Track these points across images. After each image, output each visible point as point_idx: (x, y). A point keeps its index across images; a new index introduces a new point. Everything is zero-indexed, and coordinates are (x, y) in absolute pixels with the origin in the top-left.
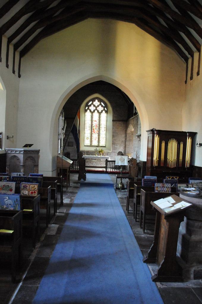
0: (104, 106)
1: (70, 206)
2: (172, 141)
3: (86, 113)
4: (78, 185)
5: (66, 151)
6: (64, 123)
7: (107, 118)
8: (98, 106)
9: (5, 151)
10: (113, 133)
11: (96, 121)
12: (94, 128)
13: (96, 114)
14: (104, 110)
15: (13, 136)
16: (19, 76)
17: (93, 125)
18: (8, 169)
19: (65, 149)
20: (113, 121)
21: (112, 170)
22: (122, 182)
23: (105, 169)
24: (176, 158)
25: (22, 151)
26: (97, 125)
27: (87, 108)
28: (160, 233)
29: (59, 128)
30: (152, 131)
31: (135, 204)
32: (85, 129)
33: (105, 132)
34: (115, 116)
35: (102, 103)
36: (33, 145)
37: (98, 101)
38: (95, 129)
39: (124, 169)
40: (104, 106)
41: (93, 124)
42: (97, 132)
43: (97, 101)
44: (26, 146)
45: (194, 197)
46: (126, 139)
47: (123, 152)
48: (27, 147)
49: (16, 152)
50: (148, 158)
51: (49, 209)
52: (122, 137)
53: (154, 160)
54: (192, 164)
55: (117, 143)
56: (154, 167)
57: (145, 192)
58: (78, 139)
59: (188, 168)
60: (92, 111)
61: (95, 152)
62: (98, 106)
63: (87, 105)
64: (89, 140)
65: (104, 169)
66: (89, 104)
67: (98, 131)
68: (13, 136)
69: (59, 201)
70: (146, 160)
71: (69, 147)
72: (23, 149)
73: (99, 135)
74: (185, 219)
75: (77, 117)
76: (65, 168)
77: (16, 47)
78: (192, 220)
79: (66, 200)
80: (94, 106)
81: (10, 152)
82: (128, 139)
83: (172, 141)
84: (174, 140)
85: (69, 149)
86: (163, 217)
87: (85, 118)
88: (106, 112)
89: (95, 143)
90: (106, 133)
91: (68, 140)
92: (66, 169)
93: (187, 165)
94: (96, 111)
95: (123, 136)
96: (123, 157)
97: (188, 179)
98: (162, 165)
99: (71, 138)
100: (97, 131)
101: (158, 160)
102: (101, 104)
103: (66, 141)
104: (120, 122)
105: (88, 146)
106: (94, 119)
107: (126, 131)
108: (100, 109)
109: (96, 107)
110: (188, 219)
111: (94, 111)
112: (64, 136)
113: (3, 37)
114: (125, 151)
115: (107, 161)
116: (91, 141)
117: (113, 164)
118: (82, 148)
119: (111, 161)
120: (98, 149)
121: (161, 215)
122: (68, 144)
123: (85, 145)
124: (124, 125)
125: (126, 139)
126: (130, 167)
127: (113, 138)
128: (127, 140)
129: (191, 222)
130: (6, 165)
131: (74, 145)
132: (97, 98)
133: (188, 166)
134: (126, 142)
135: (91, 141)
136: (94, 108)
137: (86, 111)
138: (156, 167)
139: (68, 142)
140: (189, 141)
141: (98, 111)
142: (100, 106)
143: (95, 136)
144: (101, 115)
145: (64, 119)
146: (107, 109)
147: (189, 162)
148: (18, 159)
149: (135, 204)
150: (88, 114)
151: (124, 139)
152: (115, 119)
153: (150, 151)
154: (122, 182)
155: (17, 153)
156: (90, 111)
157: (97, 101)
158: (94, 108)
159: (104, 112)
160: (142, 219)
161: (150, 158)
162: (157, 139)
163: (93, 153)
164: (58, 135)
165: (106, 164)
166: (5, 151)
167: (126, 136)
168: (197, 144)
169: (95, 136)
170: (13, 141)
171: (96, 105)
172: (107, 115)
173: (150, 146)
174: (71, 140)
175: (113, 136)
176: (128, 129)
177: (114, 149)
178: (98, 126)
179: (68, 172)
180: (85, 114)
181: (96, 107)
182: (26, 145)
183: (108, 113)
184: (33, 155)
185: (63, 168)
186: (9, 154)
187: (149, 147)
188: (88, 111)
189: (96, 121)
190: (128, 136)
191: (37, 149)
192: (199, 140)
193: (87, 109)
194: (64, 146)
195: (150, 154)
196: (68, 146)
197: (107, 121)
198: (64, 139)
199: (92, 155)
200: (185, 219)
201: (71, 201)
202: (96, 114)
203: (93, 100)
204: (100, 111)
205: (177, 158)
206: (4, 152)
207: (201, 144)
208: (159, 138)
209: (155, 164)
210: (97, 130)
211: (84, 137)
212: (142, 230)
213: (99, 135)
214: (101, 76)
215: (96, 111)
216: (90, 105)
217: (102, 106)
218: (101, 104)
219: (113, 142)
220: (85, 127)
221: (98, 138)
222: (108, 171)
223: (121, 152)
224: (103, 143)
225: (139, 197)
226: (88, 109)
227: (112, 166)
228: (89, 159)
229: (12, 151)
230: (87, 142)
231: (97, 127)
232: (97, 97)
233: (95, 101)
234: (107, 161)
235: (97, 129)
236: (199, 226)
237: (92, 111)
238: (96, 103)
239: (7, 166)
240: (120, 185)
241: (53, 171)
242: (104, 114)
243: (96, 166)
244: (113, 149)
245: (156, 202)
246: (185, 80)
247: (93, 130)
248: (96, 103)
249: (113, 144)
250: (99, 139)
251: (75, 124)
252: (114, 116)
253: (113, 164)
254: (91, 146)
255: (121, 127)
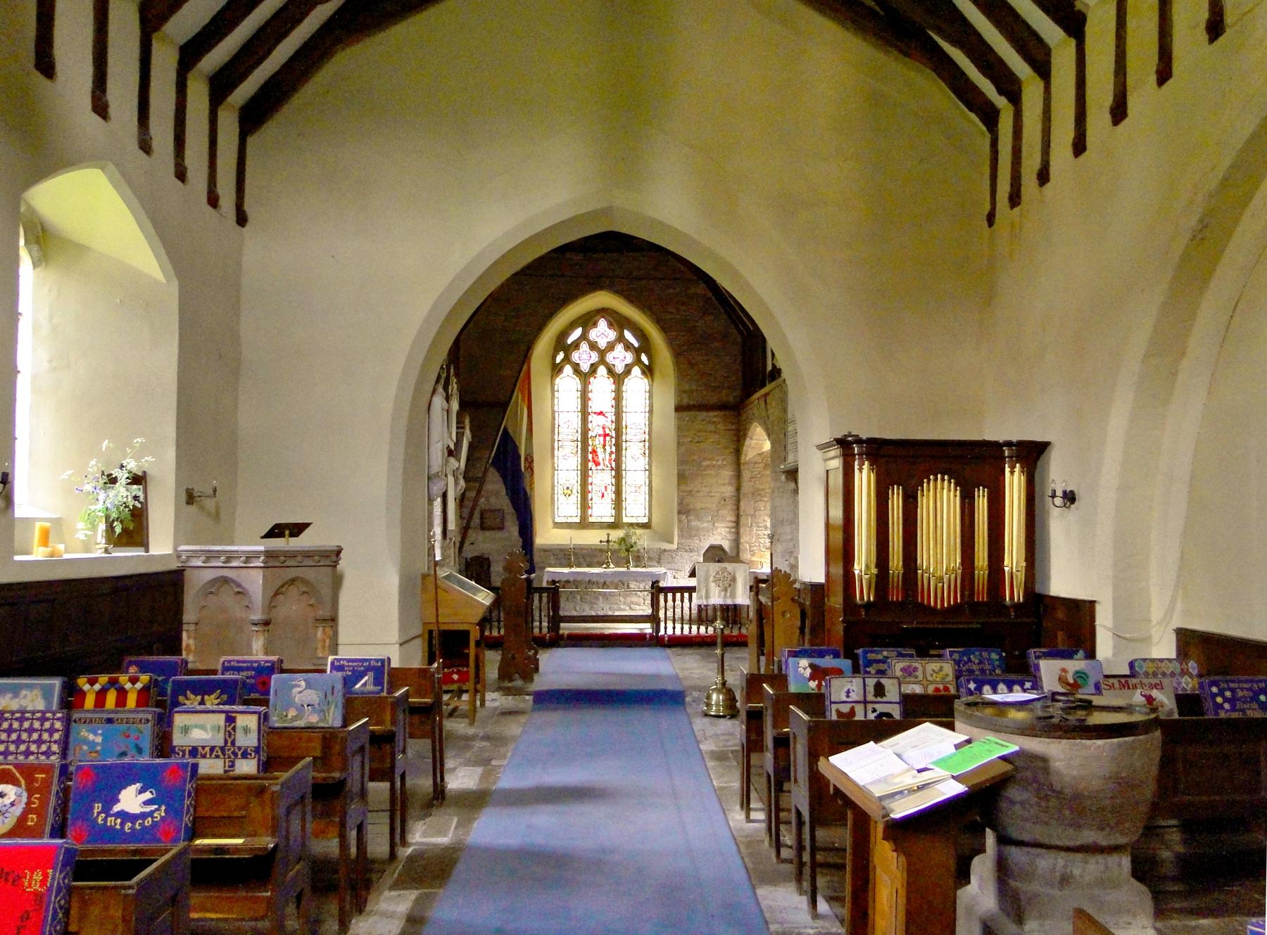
0: (636, 345)
1: (474, 801)
2: (936, 489)
3: (558, 380)
4: (525, 701)
5: (470, 552)
6: (460, 426)
7: (651, 397)
8: (611, 347)
9: (179, 557)
10: (682, 462)
11: (601, 413)
12: (597, 442)
13: (602, 386)
14: (638, 361)
15: (215, 491)
16: (242, 219)
17: (590, 434)
18: (191, 642)
19: (467, 543)
20: (679, 409)
21: (686, 627)
22: (724, 684)
23: (648, 625)
24: (959, 561)
25: (256, 555)
26: (607, 431)
27: (560, 357)
28: (870, 913)
29: (432, 449)
30: (844, 444)
31: (769, 776)
32: (556, 451)
33: (643, 462)
34: (687, 387)
35: (628, 335)
36: (306, 525)
37: (610, 325)
38: (600, 451)
39: (735, 622)
40: (636, 345)
41: (590, 426)
42: (607, 463)
43: (602, 324)
44: (276, 531)
45: (1023, 734)
46: (738, 489)
47: (726, 545)
48: (281, 535)
49: (228, 559)
50: (831, 569)
51: (403, 821)
52: (719, 483)
53: (857, 572)
54: (1038, 589)
55: (699, 506)
56: (856, 605)
57: (805, 717)
58: (525, 493)
59: (1017, 607)
60: (585, 367)
61: (601, 551)
62: (611, 347)
63: (560, 343)
64: (575, 499)
65: (647, 628)
66: (570, 341)
67: (613, 456)
68: (215, 491)
69: (422, 783)
70: (821, 578)
71: (488, 533)
72: (262, 548)
73: (618, 477)
74: (990, 838)
75: (518, 396)
76: (461, 627)
77: (221, 86)
78: (1020, 843)
79: (460, 775)
80: (593, 346)
81: (200, 564)
82: (747, 486)
83: (936, 489)
84: (943, 480)
85: (483, 543)
86: (880, 828)
87: (556, 400)
88: (648, 371)
89: (602, 510)
90: (650, 464)
91: (483, 500)
92: (466, 634)
93: (1015, 593)
94: (602, 370)
95: (727, 474)
96: (729, 566)
97: (1024, 656)
98: (895, 596)
99: (495, 492)
100: (607, 455)
101: (877, 575)
102: (621, 339)
103: (473, 508)
104: (711, 414)
105: (569, 526)
106: (594, 406)
107: (738, 452)
108: (620, 357)
109: (602, 354)
110: (1003, 840)
111: (594, 368)
112: (462, 483)
113: (154, 42)
114: (737, 542)
115: (657, 590)
116: (585, 505)
117: (682, 601)
118: (546, 535)
119: (674, 590)
120: (616, 535)
121: (872, 824)
122: (482, 518)
123: (558, 520)
124: (730, 427)
125: (738, 489)
126: (761, 611)
127: (683, 487)
128: (742, 492)
129: (1015, 854)
130: (180, 623)
131: (507, 524)
132: (603, 312)
133: (1019, 596)
134: (742, 503)
135: (585, 505)
136: (595, 357)
137: (556, 369)
138: (868, 606)
139: (482, 513)
140: (1014, 482)
141: (611, 371)
142: (620, 347)
143: (601, 479)
144: (624, 388)
145: (455, 406)
146: (650, 358)
147: (1020, 577)
148: (242, 593)
149: (769, 776)
150: (567, 383)
151: (729, 490)
152: (685, 401)
153: (838, 537)
154: (724, 684)
155: (234, 564)
156: (576, 369)
157: (602, 324)
158: (595, 357)
159: (636, 371)
160: (800, 848)
161: (838, 570)
162: (864, 479)
163: (595, 556)
164: (429, 478)
165: (655, 604)
166: (179, 557)
167: (738, 476)
168: (1054, 496)
169: (601, 479)
170: (218, 514)
171: (602, 344)
172: (651, 386)
173: (837, 513)
174: (493, 500)
175: (682, 478)
176: (747, 442)
177: (688, 533)
178: (613, 434)
179: (472, 644)
180: (553, 385)
181: (602, 354)
182: (277, 526)
183: (657, 374)
184: (310, 574)
185: (446, 627)
186: (196, 572)
187: (831, 521)
188: (568, 369)
189: (601, 413)
190: (746, 474)
191: (330, 543)
192: (1057, 474)
193: (563, 361)
194: (464, 531)
195: (841, 551)
196: (483, 527)
197: (651, 412)
198: (461, 500)
199: (589, 566)
200: (990, 838)
201: (484, 777)
202: (602, 386)
203: (587, 321)
204: (620, 369)
205: (963, 563)
206: (174, 565)
207: (1072, 492)
208: (873, 476)
209: (864, 593)
210: (612, 452)
211: (553, 489)
212: (803, 902)
213: (618, 477)
214: (607, 212)
215: (602, 370)
216: (576, 345)
217: (628, 346)
218: (621, 339)
219: (681, 503)
220: (553, 441)
221: (614, 488)
222: (662, 632)
223: (720, 548)
224: (636, 509)
225: (782, 743)
226: (567, 359)
227: (678, 611)
228: (576, 583)
229: (211, 555)
230: (568, 509)
231: (608, 438)
232: (600, 306)
233: (595, 325)
234: (657, 590)
235: (608, 448)
236: (1058, 874)
237: (585, 367)
238: (602, 333)
239: (185, 627)
240: (714, 696)
241: (404, 643)
242: (637, 384)
243: (610, 613)
244: (681, 536)
245: (838, 760)
246: (987, 208)
247: (590, 456)
248: (602, 333)
249: (684, 510)
250: (618, 492)
251: (510, 431)
252: (680, 391)
253: (682, 601)
254: (584, 524)
255: (713, 438)
